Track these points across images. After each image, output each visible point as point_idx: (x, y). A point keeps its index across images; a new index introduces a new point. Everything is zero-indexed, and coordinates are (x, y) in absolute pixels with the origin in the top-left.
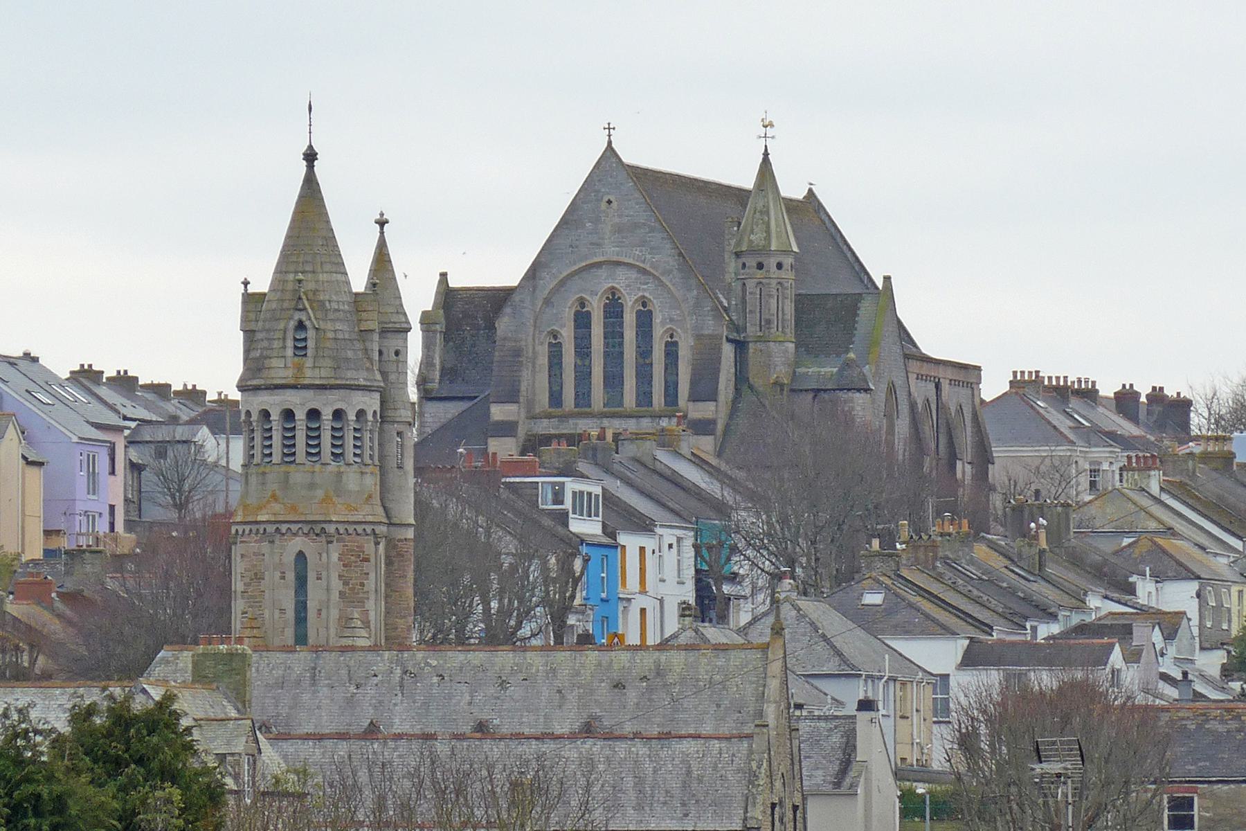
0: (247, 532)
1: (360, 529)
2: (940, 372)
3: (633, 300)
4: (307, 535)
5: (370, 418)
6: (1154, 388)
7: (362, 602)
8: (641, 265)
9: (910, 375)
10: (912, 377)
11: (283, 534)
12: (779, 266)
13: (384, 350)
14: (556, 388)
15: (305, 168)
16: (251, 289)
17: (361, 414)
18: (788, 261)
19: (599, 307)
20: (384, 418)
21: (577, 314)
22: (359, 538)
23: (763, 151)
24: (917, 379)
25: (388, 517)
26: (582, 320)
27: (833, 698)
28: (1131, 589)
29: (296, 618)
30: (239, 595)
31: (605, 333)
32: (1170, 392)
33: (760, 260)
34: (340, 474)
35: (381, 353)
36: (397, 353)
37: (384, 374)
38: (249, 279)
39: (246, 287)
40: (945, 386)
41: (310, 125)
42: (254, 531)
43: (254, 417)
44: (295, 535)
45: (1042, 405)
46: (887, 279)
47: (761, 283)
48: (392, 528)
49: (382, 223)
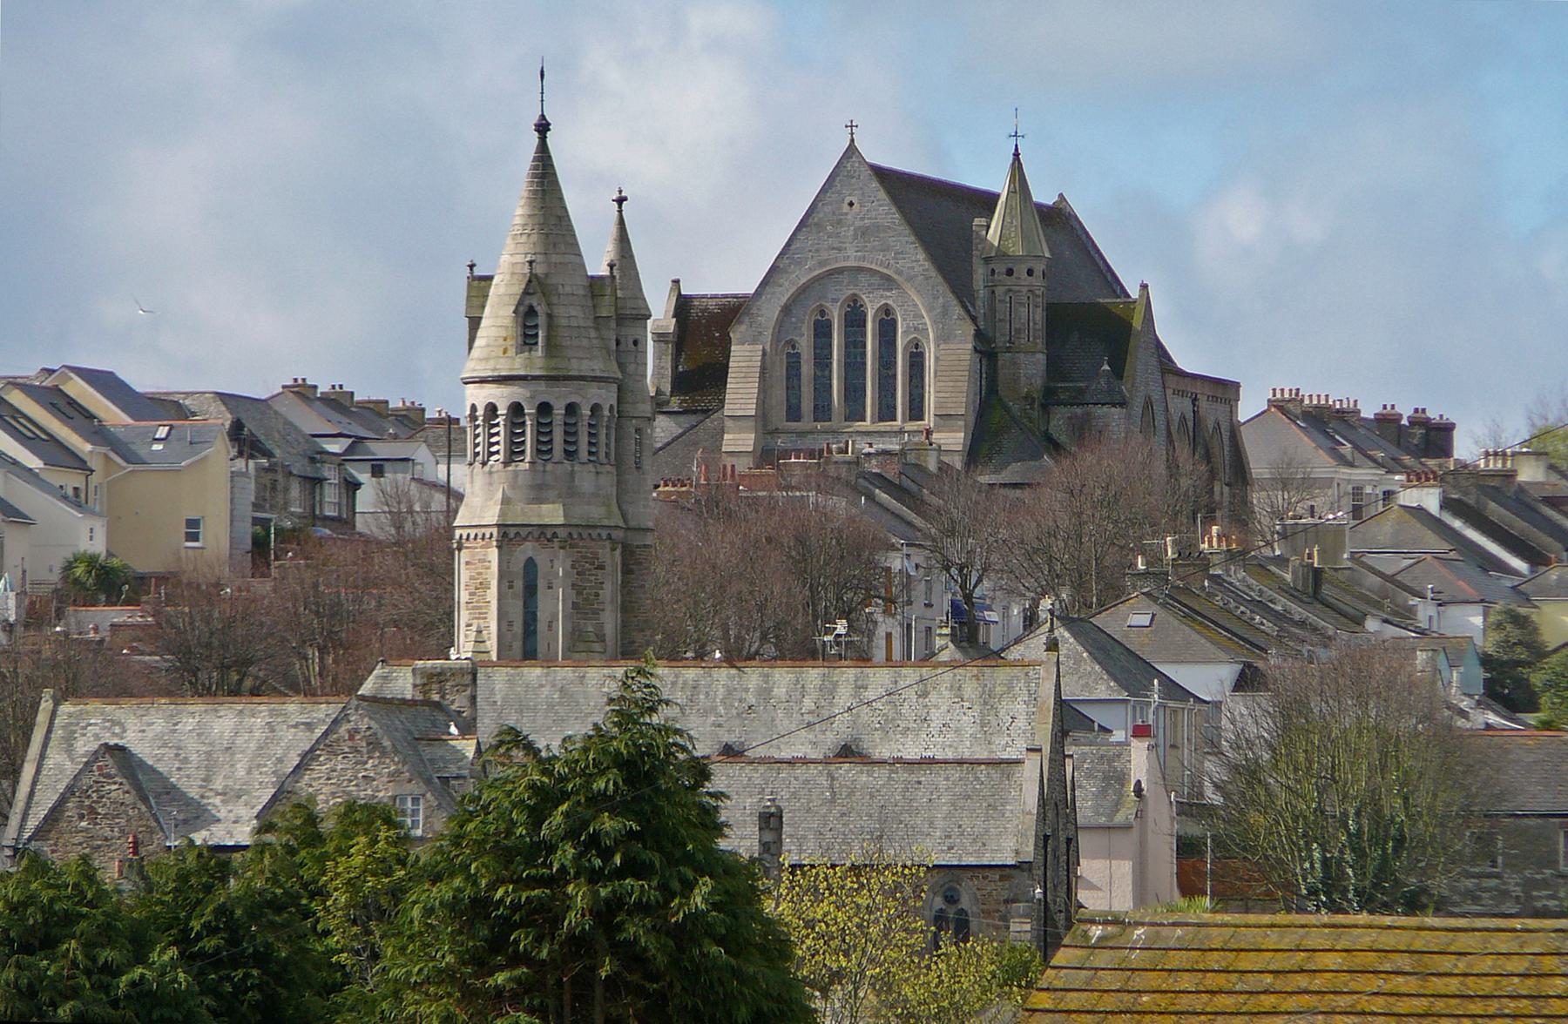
0: (472, 536)
1: (594, 534)
2: (1198, 388)
3: (876, 308)
4: (538, 540)
5: (606, 413)
6: (1416, 410)
7: (596, 612)
8: (885, 271)
9: (1167, 391)
10: (1169, 392)
11: (511, 540)
12: (1030, 272)
13: (623, 340)
14: (794, 401)
15: (537, 140)
16: (478, 272)
17: (595, 409)
18: (1039, 268)
19: (839, 315)
20: (621, 415)
21: (817, 323)
22: (593, 543)
23: (1013, 151)
24: (1174, 394)
25: (625, 521)
26: (822, 330)
27: (1099, 725)
28: (1410, 612)
29: (525, 633)
30: (463, 605)
31: (846, 344)
32: (1432, 414)
33: (1010, 265)
34: (572, 474)
35: (618, 343)
36: (635, 343)
37: (621, 366)
38: (474, 262)
39: (471, 270)
40: (1203, 403)
41: (542, 93)
42: (480, 536)
43: (480, 412)
44: (525, 539)
45: (1302, 425)
46: (1144, 287)
47: (1010, 290)
48: (629, 534)
49: (620, 201)
